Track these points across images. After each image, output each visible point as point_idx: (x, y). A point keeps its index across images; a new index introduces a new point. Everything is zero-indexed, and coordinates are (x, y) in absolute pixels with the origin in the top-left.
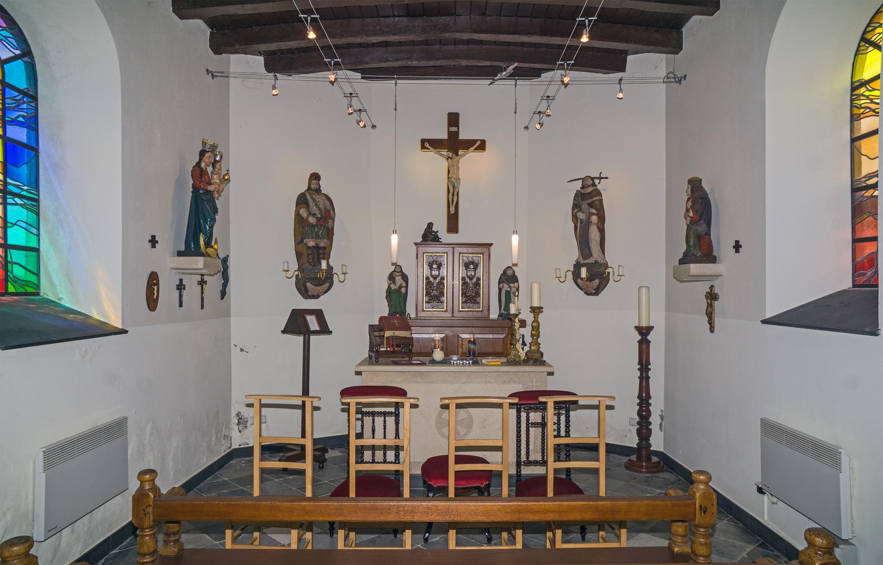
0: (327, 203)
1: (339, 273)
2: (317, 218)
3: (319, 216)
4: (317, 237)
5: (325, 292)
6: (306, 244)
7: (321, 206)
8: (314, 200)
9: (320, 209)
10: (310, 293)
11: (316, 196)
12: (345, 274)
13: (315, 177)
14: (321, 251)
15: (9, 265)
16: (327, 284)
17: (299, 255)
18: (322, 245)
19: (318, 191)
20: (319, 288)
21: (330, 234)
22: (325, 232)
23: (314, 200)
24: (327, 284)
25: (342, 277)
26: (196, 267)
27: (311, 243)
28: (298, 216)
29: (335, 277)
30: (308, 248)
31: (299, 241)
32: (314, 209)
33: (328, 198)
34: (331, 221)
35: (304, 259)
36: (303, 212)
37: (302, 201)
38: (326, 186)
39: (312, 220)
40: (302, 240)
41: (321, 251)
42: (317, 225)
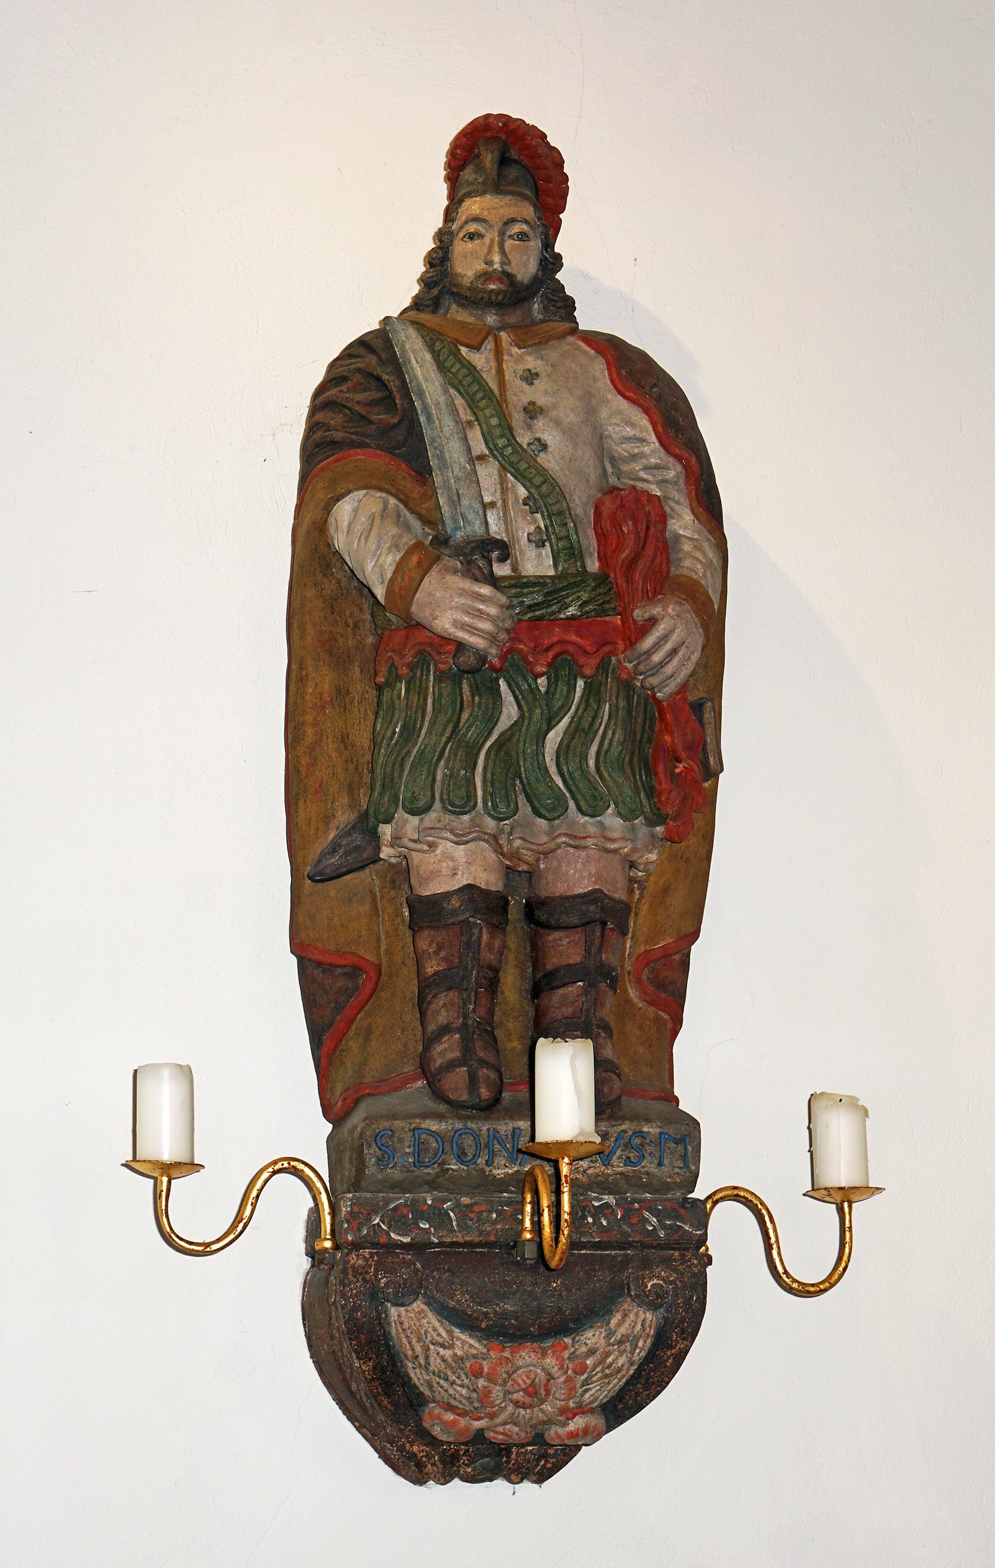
0: (629, 426)
1: (784, 1190)
2: (519, 583)
3: (537, 563)
4: (513, 775)
5: (620, 1408)
6: (401, 873)
7: (558, 452)
8: (482, 399)
9: (545, 496)
10: (440, 1423)
11: (518, 369)
12: (844, 1199)
13: (508, 165)
14: (565, 949)
15: (605, 441)
16: (635, 1322)
17: (334, 994)
18: (575, 875)
19: (537, 300)
20: (530, 1362)
21: (673, 762)
22: (607, 733)
23: (482, 399)
24: (635, 1322)
25: (808, 1238)
26: (534, 841)
27: (453, 861)
28: (315, 559)
29: (729, 1232)
30: (426, 912)
31: (334, 845)
32: (483, 498)
33: (635, 373)
34: (670, 627)
35: (388, 1036)
36: (369, 536)
37: (361, 417)
38: (611, 263)
39: (458, 610)
40: (366, 826)
41: (565, 949)
42: (513, 663)
